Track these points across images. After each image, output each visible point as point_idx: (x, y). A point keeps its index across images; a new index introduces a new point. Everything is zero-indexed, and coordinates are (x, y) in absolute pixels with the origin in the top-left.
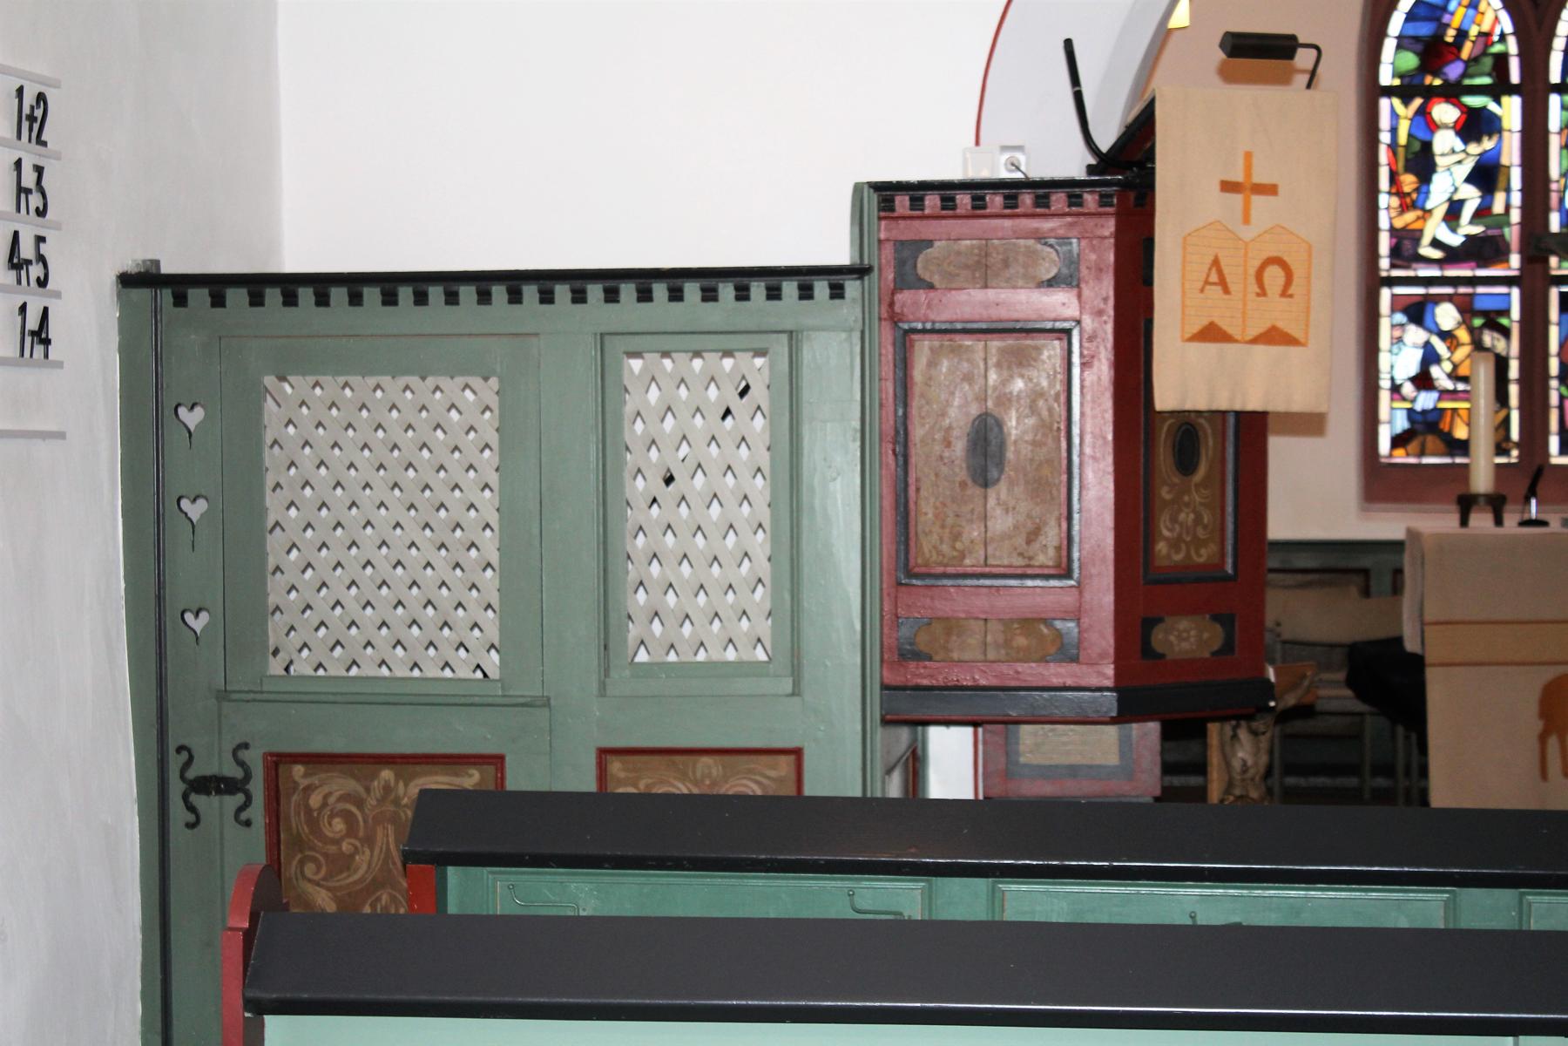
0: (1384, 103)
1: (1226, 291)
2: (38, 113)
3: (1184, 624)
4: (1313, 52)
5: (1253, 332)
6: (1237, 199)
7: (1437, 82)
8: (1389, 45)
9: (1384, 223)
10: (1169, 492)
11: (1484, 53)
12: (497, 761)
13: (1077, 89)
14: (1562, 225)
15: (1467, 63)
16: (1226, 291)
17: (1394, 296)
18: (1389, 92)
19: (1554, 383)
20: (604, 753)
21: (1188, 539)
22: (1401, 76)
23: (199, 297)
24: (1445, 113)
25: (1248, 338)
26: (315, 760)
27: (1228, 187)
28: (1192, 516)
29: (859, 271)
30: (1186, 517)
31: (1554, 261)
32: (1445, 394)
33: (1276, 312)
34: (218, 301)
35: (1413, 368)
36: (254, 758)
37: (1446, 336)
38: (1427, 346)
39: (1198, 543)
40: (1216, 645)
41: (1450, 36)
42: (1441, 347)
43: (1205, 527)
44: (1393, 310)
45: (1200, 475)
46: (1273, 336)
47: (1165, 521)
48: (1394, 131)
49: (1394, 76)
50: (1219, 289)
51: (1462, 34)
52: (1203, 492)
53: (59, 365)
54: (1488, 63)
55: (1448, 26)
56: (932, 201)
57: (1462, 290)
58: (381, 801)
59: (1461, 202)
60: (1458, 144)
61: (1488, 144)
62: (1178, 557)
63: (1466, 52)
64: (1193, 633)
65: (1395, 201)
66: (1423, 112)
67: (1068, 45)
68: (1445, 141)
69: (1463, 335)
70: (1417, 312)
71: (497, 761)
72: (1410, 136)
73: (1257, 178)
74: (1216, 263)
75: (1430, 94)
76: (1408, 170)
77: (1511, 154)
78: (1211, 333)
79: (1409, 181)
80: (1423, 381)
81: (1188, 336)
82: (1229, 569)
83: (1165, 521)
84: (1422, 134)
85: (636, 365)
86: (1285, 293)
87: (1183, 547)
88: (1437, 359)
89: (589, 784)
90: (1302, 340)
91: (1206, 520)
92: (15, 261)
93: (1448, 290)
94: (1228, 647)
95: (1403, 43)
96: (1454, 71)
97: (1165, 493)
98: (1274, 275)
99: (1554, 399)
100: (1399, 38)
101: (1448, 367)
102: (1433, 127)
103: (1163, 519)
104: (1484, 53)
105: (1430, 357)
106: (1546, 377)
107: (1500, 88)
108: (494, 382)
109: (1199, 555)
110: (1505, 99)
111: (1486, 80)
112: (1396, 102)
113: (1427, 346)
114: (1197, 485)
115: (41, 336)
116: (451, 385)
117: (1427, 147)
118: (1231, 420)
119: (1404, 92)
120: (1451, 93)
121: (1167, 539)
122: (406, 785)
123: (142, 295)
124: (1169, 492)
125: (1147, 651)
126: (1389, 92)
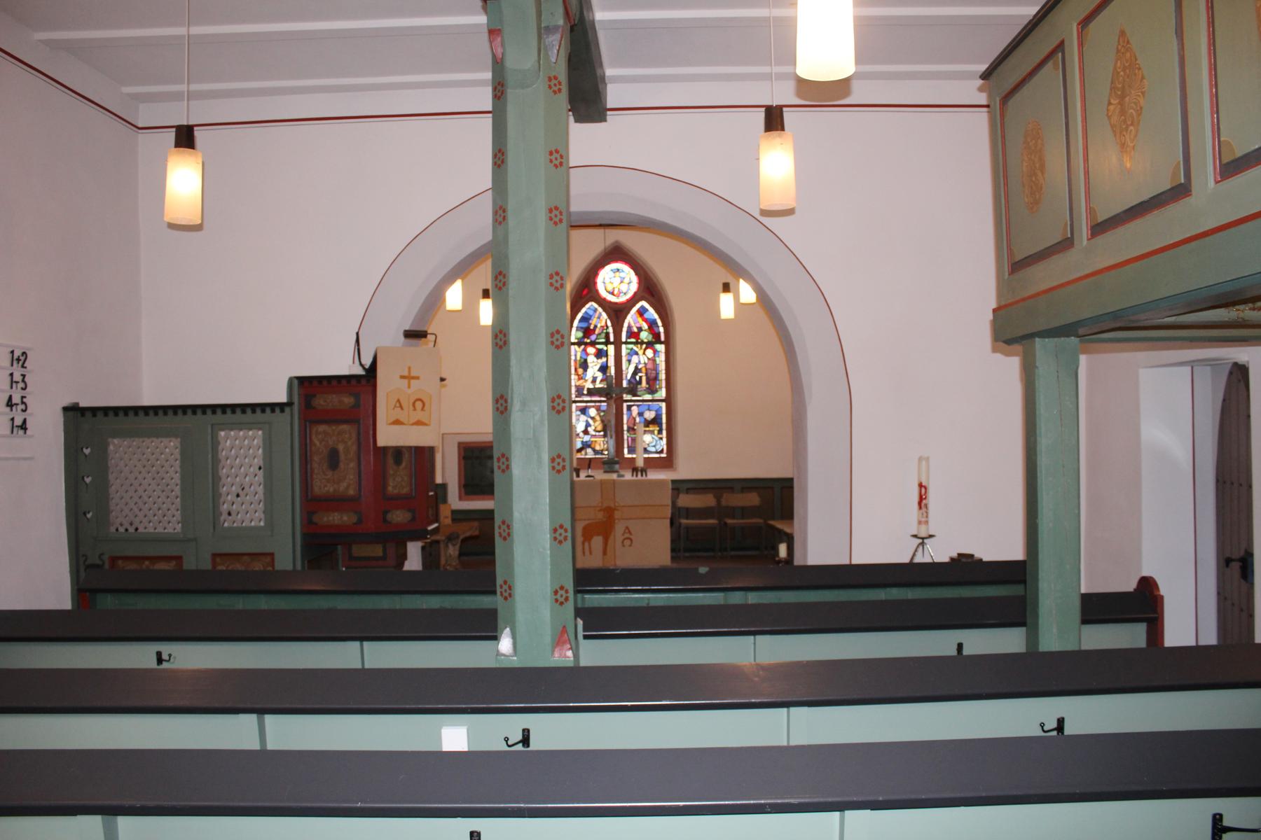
0: (573, 347)
2: (22, 358)
3: (398, 512)
4: (434, 336)
5: (412, 422)
6: (406, 381)
7: (588, 341)
8: (574, 329)
9: (573, 384)
11: (602, 332)
12: (179, 559)
14: (627, 384)
15: (597, 335)
17: (577, 407)
18: (574, 344)
19: (625, 432)
20: (215, 555)
22: (578, 339)
23: (89, 414)
24: (591, 350)
25: (411, 422)
26: (127, 558)
27: (402, 377)
29: (289, 404)
31: (624, 395)
32: (593, 436)
33: (419, 415)
34: (94, 415)
35: (583, 429)
36: (106, 558)
37: (593, 418)
38: (587, 421)
41: (592, 327)
42: (591, 422)
44: (576, 410)
45: (404, 464)
46: (419, 423)
48: (576, 355)
49: (576, 338)
50: (399, 409)
51: (596, 327)
53: (32, 436)
54: (603, 335)
55: (591, 324)
57: (597, 404)
59: (596, 377)
60: (595, 359)
61: (604, 360)
62: (396, 491)
63: (597, 332)
65: (577, 377)
66: (585, 350)
68: (591, 359)
69: (598, 418)
70: (583, 411)
71: (179, 559)
72: (581, 357)
73: (412, 374)
75: (586, 344)
76: (580, 367)
77: (611, 363)
78: (397, 422)
79: (580, 371)
80: (586, 432)
81: (389, 422)
82: (414, 495)
84: (584, 357)
85: (222, 433)
86: (423, 409)
88: (590, 425)
89: (209, 567)
92: (10, 404)
93: (593, 404)
94: (414, 519)
95: (578, 329)
96: (593, 337)
97: (391, 472)
98: (419, 405)
99: (625, 437)
100: (577, 327)
101: (593, 428)
102: (587, 354)
104: (602, 332)
105: (588, 425)
106: (623, 430)
107: (607, 343)
108: (179, 440)
110: (609, 346)
111: (603, 340)
112: (576, 347)
113: (587, 421)
115: (23, 426)
116: (165, 441)
117: (586, 361)
118: (413, 449)
119: (579, 344)
120: (593, 344)
123: (71, 414)
125: (385, 520)
126: (574, 344)
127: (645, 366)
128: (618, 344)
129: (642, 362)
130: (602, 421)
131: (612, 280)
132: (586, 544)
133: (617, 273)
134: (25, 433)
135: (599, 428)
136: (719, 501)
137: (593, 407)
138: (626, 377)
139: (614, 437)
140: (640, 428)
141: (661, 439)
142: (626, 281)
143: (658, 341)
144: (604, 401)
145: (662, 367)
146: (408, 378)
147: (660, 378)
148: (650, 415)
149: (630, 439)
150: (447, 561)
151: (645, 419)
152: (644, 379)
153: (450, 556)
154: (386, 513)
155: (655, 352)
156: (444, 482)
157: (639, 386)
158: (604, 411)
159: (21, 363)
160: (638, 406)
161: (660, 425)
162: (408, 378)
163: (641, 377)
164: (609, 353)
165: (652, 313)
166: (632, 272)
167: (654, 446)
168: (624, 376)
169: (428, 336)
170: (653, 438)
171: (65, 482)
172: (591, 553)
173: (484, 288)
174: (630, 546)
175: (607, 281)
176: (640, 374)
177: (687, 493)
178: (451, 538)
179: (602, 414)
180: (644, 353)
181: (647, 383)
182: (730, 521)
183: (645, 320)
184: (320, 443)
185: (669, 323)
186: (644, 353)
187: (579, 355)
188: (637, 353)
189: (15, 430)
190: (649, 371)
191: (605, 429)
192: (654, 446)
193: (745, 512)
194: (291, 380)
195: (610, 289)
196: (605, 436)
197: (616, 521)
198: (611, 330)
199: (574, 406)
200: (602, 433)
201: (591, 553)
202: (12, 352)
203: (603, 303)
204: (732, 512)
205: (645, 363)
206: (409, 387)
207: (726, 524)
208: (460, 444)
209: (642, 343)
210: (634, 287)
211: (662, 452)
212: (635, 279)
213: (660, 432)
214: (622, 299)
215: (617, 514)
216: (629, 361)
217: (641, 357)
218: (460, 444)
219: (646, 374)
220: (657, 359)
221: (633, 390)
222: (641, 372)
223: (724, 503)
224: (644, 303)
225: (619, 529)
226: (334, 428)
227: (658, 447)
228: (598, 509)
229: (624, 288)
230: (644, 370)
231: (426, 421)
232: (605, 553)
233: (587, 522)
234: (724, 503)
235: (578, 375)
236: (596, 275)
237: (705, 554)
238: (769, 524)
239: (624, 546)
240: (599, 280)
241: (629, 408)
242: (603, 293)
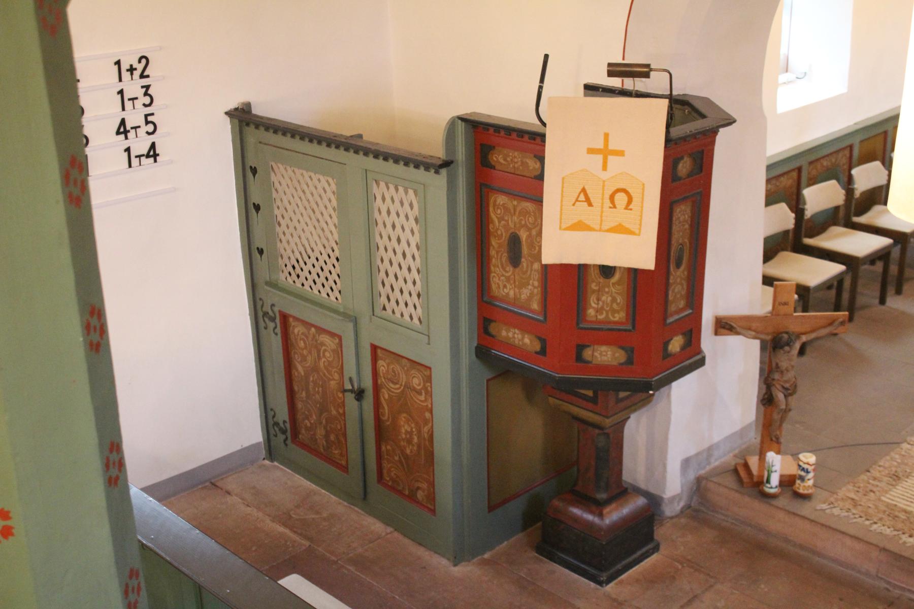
1: (590, 205)
3: (604, 348)
10: (596, 286)
13: (541, 84)
16: (590, 205)
21: (608, 309)
28: (610, 299)
30: (606, 298)
36: (276, 309)
39: (614, 311)
40: (623, 360)
43: (618, 304)
46: (619, 229)
47: (593, 299)
52: (618, 287)
56: (492, 130)
58: (312, 340)
64: (609, 353)
67: (546, 56)
73: (600, 158)
74: (584, 190)
78: (580, 226)
83: (593, 299)
86: (627, 207)
87: (604, 312)
90: (637, 231)
91: (619, 301)
92: (122, 130)
97: (594, 286)
98: (621, 199)
103: (592, 299)
109: (614, 317)
114: (613, 284)
121: (594, 308)
122: (319, 336)
124: (596, 286)
125: (579, 358)
134: (155, 161)
146: (606, 152)
154: (581, 348)
159: (137, 74)
162: (606, 152)
169: (652, 73)
171: (238, 206)
184: (499, 222)
189: (135, 162)
194: (452, 124)
202: (118, 63)
206: (605, 168)
226: (515, 203)
231: (634, 227)
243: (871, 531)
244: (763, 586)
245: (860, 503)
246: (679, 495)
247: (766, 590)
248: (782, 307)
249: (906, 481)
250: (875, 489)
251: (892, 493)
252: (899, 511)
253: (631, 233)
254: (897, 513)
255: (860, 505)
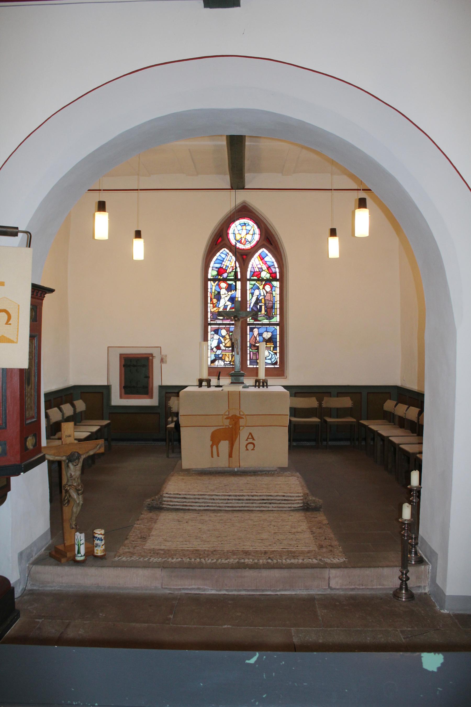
0: (209, 282)
11: (232, 271)
18: (210, 280)
24: (223, 285)
35: (216, 345)
37: (223, 337)
42: (222, 340)
48: (211, 289)
54: (233, 274)
68: (223, 291)
69: (227, 337)
70: (216, 332)
75: (219, 280)
79: (215, 301)
80: (218, 347)
84: (219, 290)
88: (222, 343)
90: (15, 341)
96: (225, 275)
99: (248, 352)
101: (224, 344)
102: (221, 288)
105: (220, 342)
107: (236, 279)
112: (212, 282)
117: (219, 293)
119: (214, 280)
120: (225, 280)
126: (210, 280)
127: (264, 298)
128: (244, 280)
129: (262, 294)
130: (231, 339)
131: (240, 232)
132: (215, 447)
133: (244, 227)
135: (228, 345)
136: (320, 404)
137: (224, 328)
138: (250, 306)
139: (240, 353)
140: (262, 346)
141: (276, 353)
142: (251, 232)
143: (275, 279)
144: (233, 324)
145: (277, 298)
147: (276, 307)
148: (267, 335)
149: (251, 353)
150: (68, 481)
151: (264, 338)
152: (263, 307)
153: (71, 476)
155: (272, 287)
156: (109, 384)
157: (259, 313)
158: (232, 332)
160: (258, 328)
161: (275, 343)
163: (261, 306)
164: (237, 288)
165: (270, 258)
166: (256, 226)
167: (270, 359)
168: (248, 306)
170: (269, 353)
172: (218, 456)
173: (136, 230)
174: (253, 450)
175: (236, 232)
176: (260, 304)
177: (295, 397)
178: (72, 458)
179: (231, 334)
180: (264, 288)
181: (265, 311)
182: (329, 420)
183: (265, 263)
185: (283, 264)
186: (264, 288)
187: (214, 288)
188: (258, 288)
190: (267, 302)
191: (233, 346)
192: (270, 359)
193: (340, 412)
195: (238, 237)
196: (233, 351)
197: (241, 428)
198: (238, 270)
199: (209, 327)
200: (230, 349)
201: (218, 456)
203: (234, 250)
204: (330, 412)
205: (264, 295)
207: (326, 421)
208: (121, 355)
209: (262, 280)
210: (257, 237)
211: (276, 363)
212: (257, 231)
213: (275, 348)
214: (248, 246)
215: (242, 422)
216: (252, 294)
217: (261, 290)
218: (121, 355)
219: (265, 304)
220: (274, 292)
221: (255, 314)
222: (262, 303)
223: (324, 405)
224: (263, 250)
225: (244, 434)
227: (273, 360)
228: (226, 417)
229: (249, 237)
230: (263, 301)
232: (230, 456)
233: (213, 429)
234: (324, 405)
235: (213, 303)
236: (229, 227)
237: (308, 444)
238: (360, 423)
239: (247, 450)
240: (231, 231)
241: (252, 330)
242: (233, 242)
243: (151, 562)
244: (101, 614)
245: (134, 553)
246: (19, 580)
247: (104, 615)
248: (68, 438)
249: (150, 538)
250: (137, 545)
251: (147, 544)
252: (158, 551)
253: (12, 342)
254: (157, 552)
255: (135, 553)
